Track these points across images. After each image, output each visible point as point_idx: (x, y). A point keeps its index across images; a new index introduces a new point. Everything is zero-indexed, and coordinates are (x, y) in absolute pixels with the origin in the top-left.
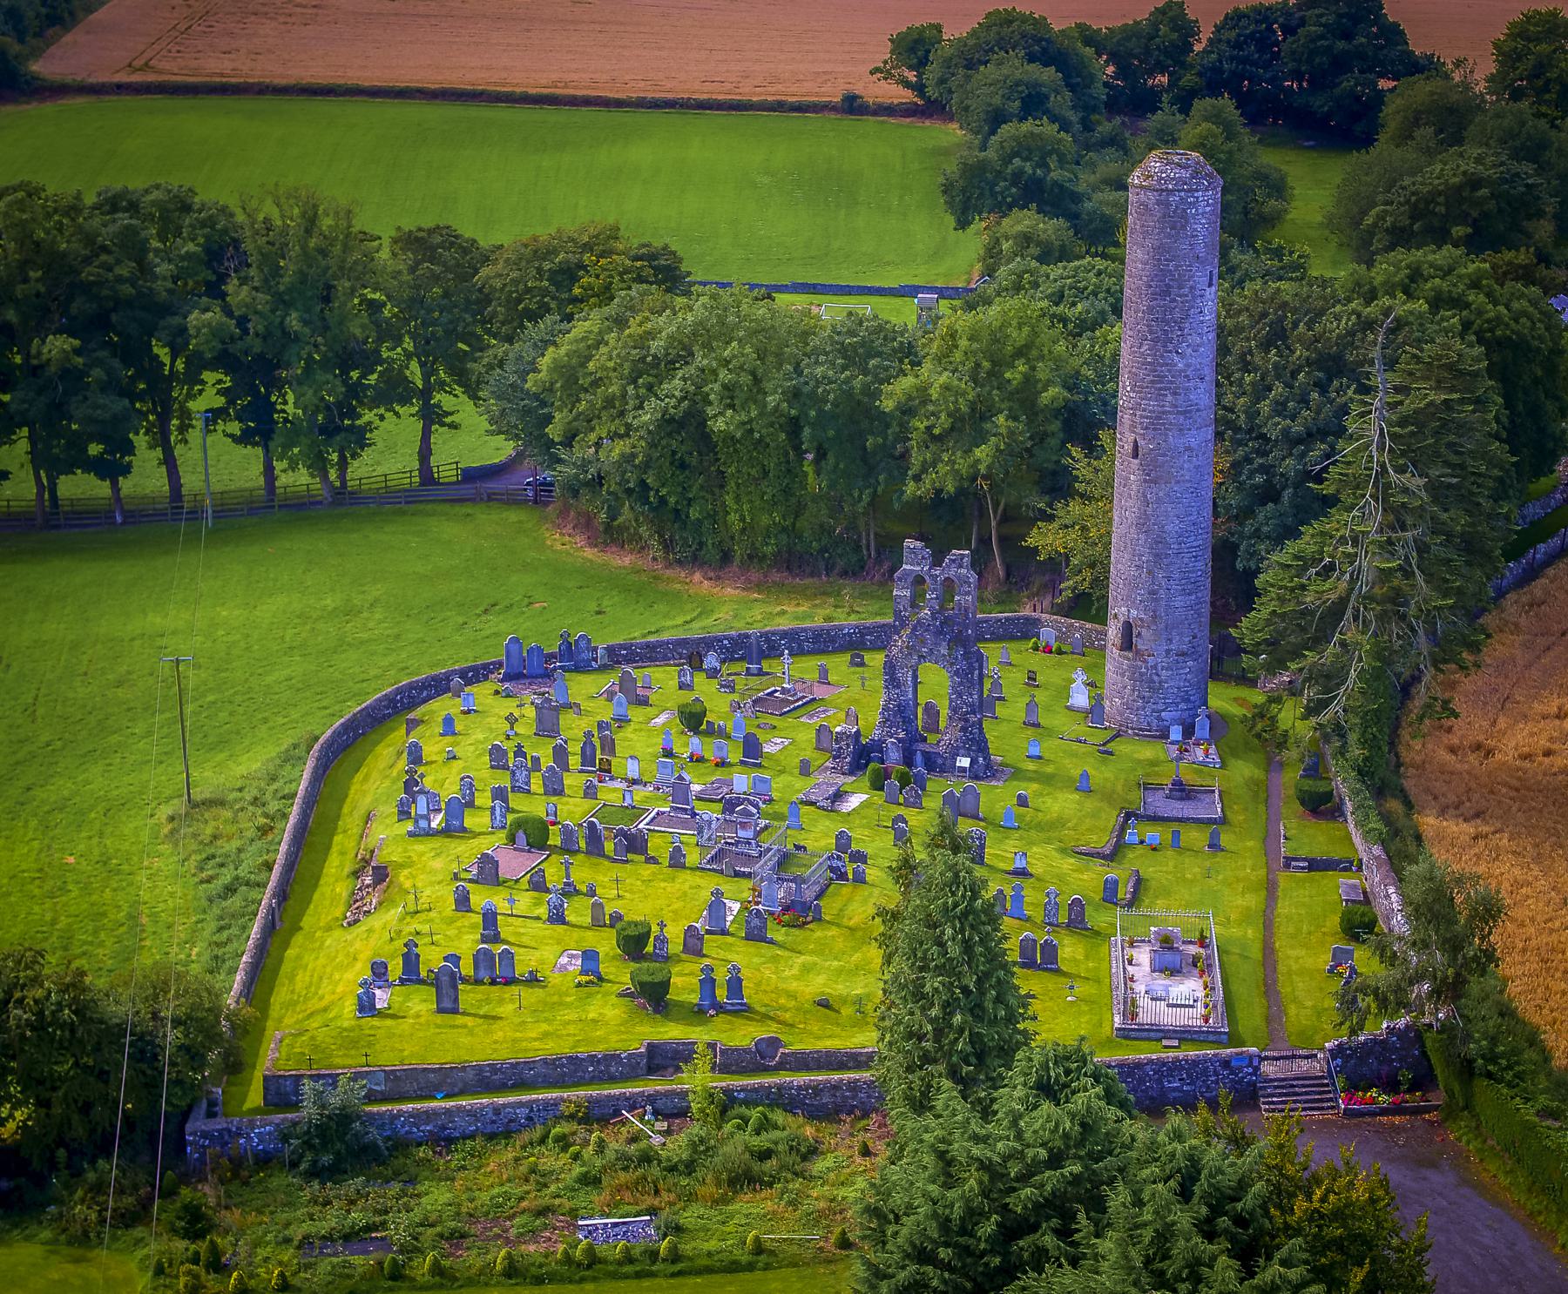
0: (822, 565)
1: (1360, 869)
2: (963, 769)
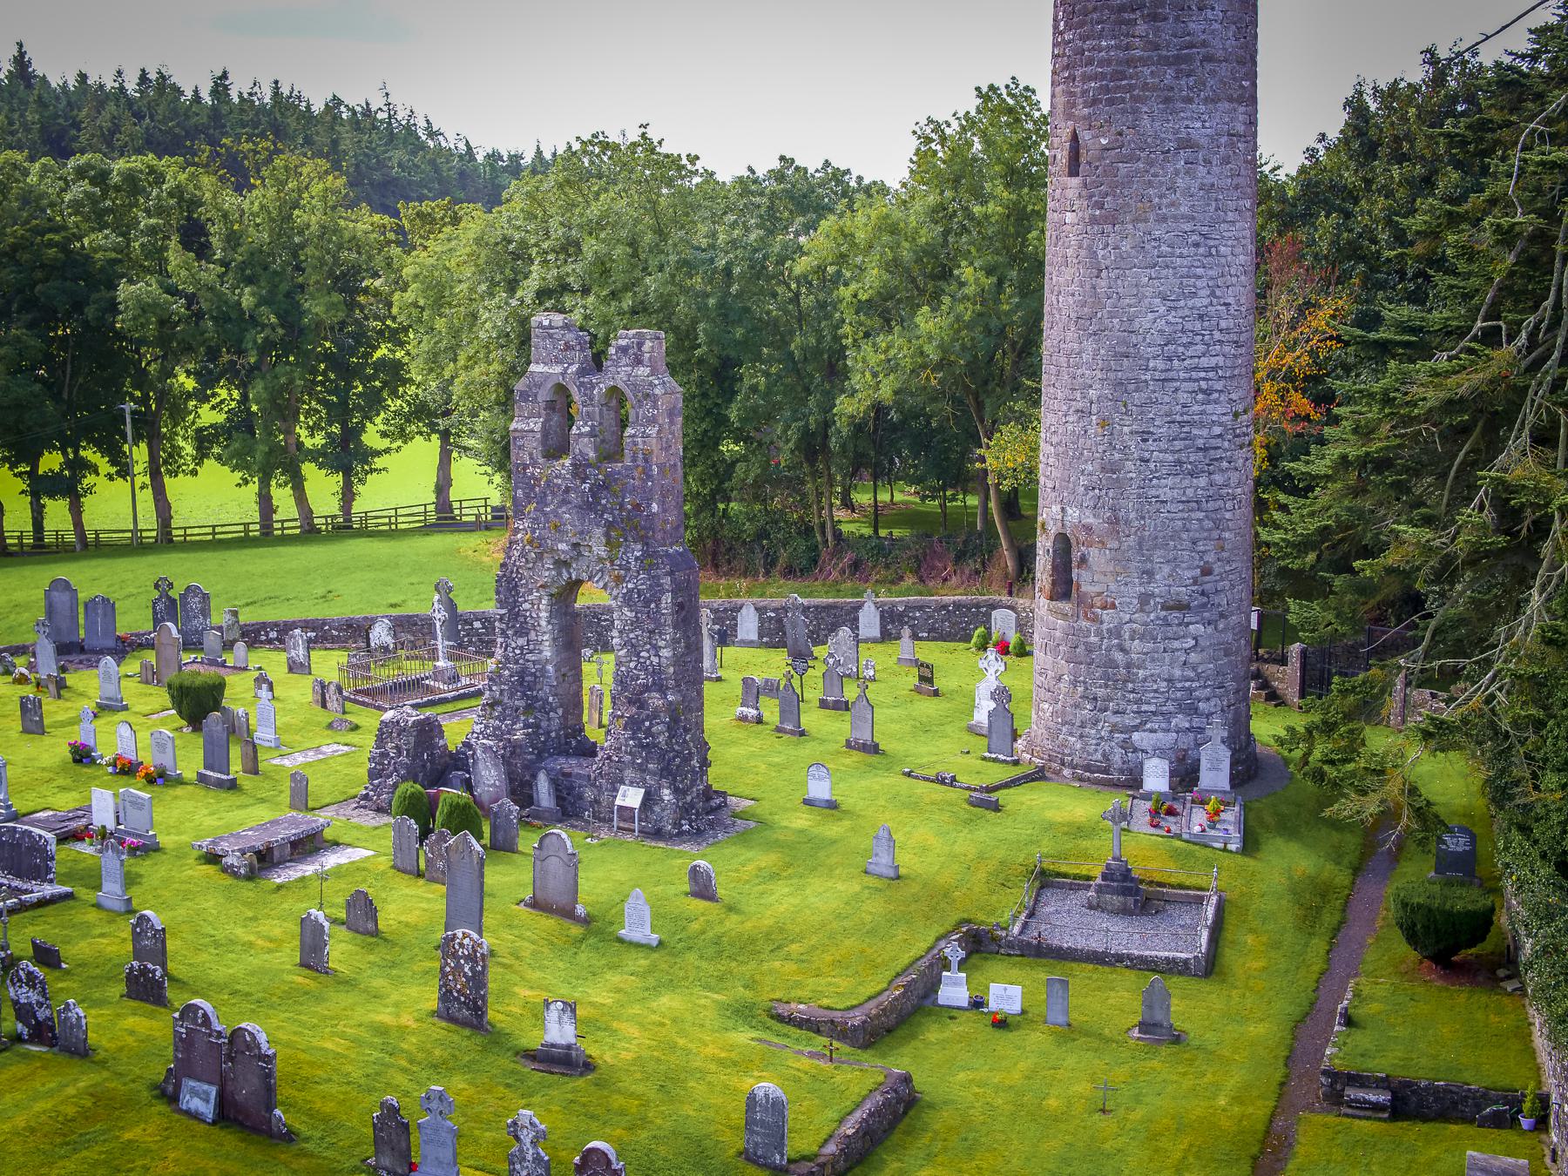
0: (759, 559)
1: (1542, 1124)
2: (625, 812)
